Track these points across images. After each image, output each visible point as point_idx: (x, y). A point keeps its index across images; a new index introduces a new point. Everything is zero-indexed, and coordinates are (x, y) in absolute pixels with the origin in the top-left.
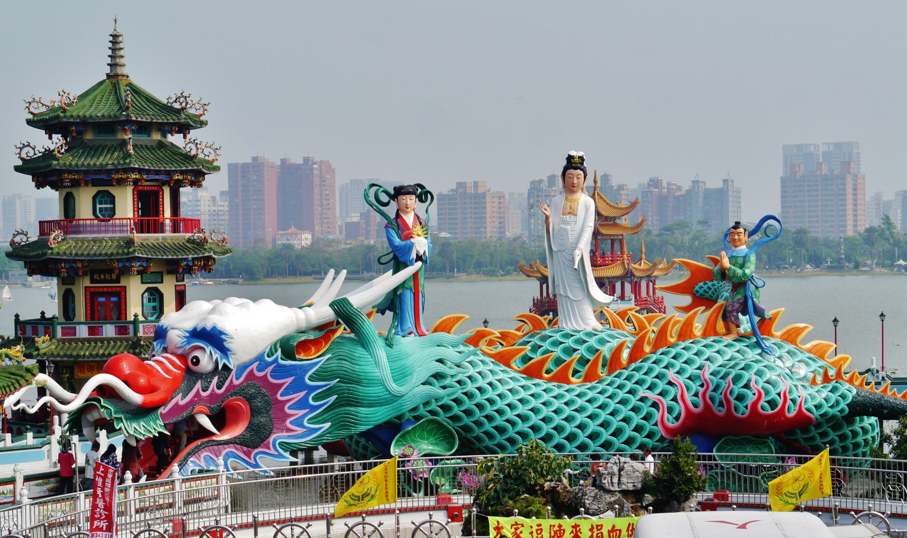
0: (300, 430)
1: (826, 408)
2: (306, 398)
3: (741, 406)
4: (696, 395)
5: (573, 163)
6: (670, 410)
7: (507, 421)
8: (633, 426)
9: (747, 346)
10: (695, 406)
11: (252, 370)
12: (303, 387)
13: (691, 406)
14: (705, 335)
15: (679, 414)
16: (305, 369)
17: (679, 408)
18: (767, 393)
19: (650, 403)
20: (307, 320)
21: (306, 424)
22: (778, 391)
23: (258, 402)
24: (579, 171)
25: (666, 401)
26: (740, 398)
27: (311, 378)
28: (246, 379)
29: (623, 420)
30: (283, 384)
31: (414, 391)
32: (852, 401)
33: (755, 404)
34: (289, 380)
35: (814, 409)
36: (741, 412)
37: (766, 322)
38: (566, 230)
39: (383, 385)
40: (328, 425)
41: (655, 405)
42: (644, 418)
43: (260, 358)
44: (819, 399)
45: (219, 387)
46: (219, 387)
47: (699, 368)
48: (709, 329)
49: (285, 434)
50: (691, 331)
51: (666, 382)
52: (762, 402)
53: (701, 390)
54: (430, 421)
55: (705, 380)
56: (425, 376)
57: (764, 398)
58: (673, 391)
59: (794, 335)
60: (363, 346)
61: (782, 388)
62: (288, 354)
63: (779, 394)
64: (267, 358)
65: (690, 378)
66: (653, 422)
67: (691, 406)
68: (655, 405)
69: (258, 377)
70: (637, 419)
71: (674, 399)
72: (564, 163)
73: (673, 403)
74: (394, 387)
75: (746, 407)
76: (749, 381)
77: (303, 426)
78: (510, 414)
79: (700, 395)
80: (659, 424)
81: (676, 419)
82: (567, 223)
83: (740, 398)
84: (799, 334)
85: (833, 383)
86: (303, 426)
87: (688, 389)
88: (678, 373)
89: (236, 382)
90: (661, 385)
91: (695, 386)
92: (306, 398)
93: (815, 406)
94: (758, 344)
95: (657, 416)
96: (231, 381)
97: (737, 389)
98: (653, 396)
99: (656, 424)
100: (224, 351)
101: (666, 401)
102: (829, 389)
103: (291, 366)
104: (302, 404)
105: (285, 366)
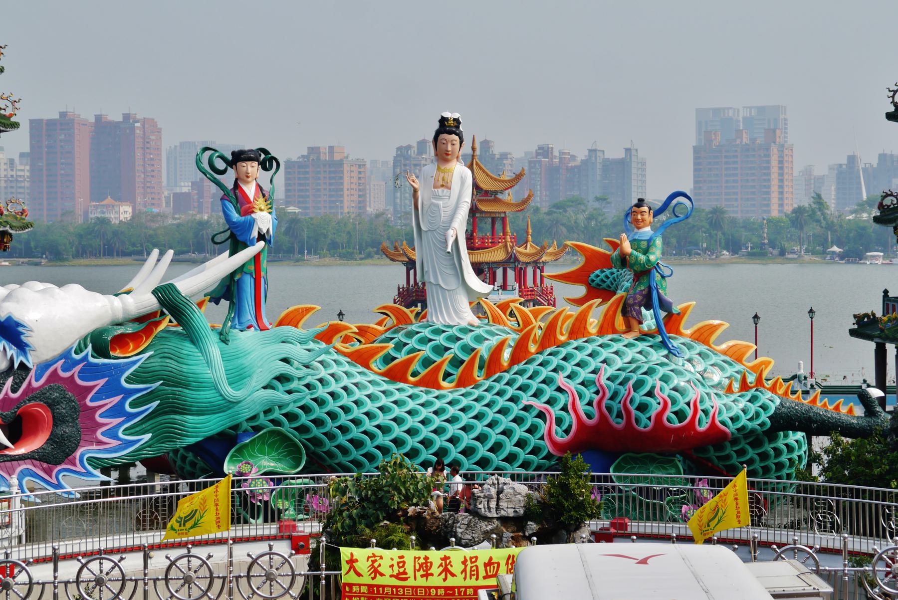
0: (114, 443)
1: (743, 421)
2: (121, 403)
3: (643, 417)
4: (590, 404)
6: (559, 421)
7: (365, 432)
8: (515, 439)
9: (651, 346)
10: (589, 416)
11: (56, 370)
13: (584, 417)
14: (601, 332)
15: (570, 426)
17: (569, 419)
18: (674, 402)
19: (535, 413)
20: (125, 310)
21: (121, 435)
22: (687, 400)
23: (63, 409)
24: (454, 137)
26: (643, 408)
28: (48, 381)
29: (503, 433)
31: (252, 397)
32: (775, 413)
33: (660, 415)
34: (102, 382)
35: (730, 422)
36: (643, 425)
38: (438, 206)
40: (148, 437)
41: (541, 415)
42: (529, 431)
44: (736, 410)
46: (14, 390)
47: (594, 372)
48: (605, 326)
49: (94, 447)
50: (585, 328)
51: (554, 387)
52: (668, 413)
53: (596, 398)
54: (272, 432)
55: (601, 386)
56: (267, 378)
57: (671, 409)
58: (562, 399)
59: (706, 334)
60: (193, 342)
61: (691, 396)
62: (101, 350)
63: (688, 404)
64: (74, 356)
65: (582, 384)
66: (539, 436)
67: (584, 417)
68: (541, 415)
70: (519, 432)
71: (564, 409)
72: (436, 126)
73: (563, 413)
74: (230, 392)
75: (649, 419)
78: (368, 425)
79: (595, 404)
80: (546, 438)
81: (567, 432)
82: (439, 197)
83: (643, 408)
87: (580, 396)
88: (569, 377)
89: (35, 384)
90: (549, 392)
92: (121, 403)
93: (731, 419)
95: (543, 428)
96: (30, 383)
98: (538, 404)
99: (542, 438)
101: (555, 411)
103: (104, 365)
105: (96, 365)
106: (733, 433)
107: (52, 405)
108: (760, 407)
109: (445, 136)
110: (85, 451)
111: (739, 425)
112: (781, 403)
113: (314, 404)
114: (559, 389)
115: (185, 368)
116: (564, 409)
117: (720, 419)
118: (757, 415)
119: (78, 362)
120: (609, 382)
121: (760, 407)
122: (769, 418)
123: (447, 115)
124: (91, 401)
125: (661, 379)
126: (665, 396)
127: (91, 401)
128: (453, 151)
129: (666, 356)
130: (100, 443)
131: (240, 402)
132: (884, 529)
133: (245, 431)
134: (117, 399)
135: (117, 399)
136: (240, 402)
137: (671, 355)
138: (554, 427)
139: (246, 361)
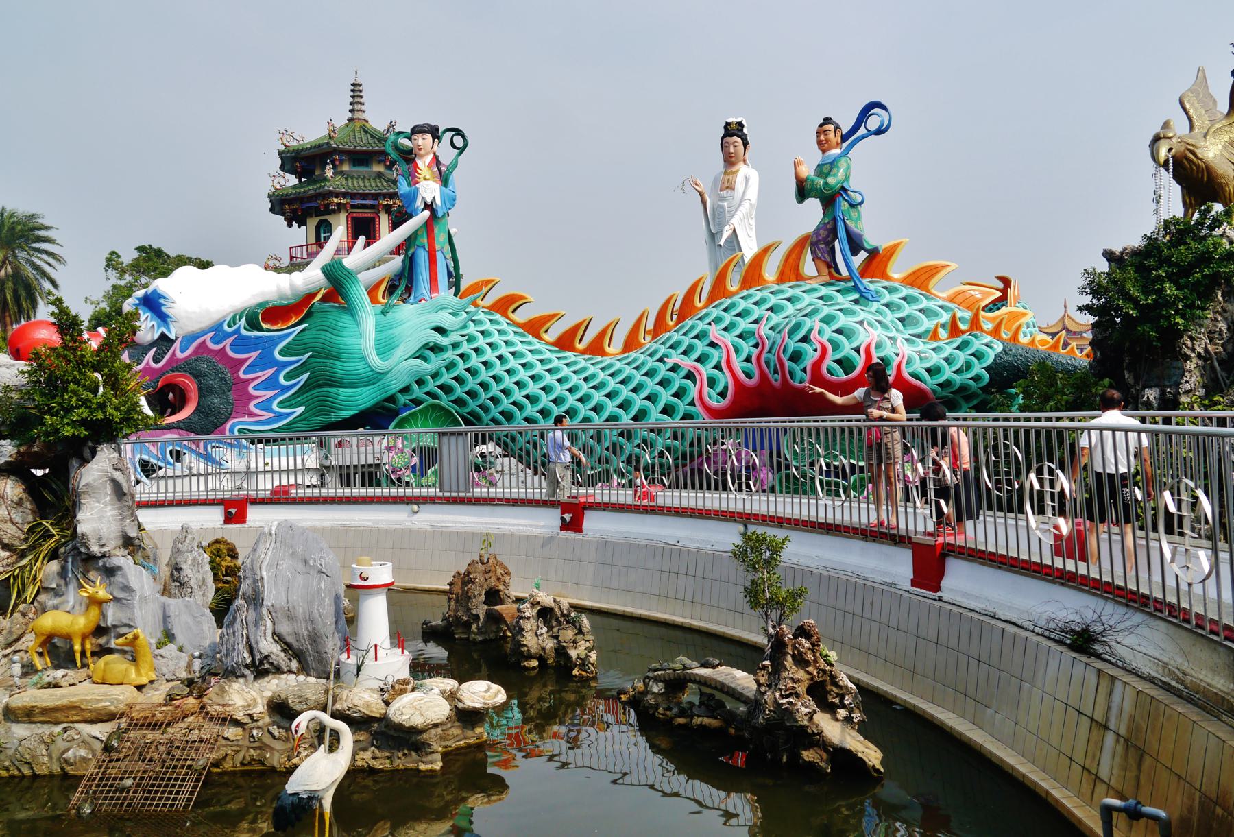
0: (267, 415)
1: (947, 374)
2: (274, 377)
3: (797, 369)
4: (748, 360)
5: (733, 130)
6: (712, 382)
7: (514, 403)
8: (661, 406)
9: (838, 291)
10: (748, 376)
11: (204, 342)
12: (273, 363)
13: (742, 377)
14: (781, 279)
15: (726, 388)
16: (274, 342)
17: (724, 379)
18: (836, 346)
19: (683, 373)
20: (292, 286)
21: (275, 407)
22: (855, 345)
23: (213, 381)
24: (735, 138)
25: (705, 370)
26: (796, 357)
27: (282, 353)
28: (195, 352)
29: (648, 398)
30: (246, 359)
31: (400, 367)
32: (995, 362)
33: (817, 364)
34: (255, 354)
35: (926, 375)
36: (798, 379)
37: (878, 259)
38: (722, 207)
39: (363, 358)
40: (303, 408)
41: (690, 376)
42: (676, 395)
43: (217, 328)
44: (935, 359)
45: (156, 360)
46: (156, 360)
47: (756, 322)
48: (787, 272)
49: (246, 419)
50: (760, 275)
51: (707, 342)
52: (828, 362)
53: (755, 352)
54: (433, 406)
55: (760, 337)
56: (414, 347)
57: (831, 356)
58: (715, 356)
59: (923, 277)
60: (352, 316)
61: (862, 339)
62: (253, 324)
63: (857, 350)
64: (226, 328)
65: (740, 336)
66: (689, 400)
67: (742, 377)
68: (690, 376)
69: (212, 351)
70: (665, 397)
71: (717, 367)
72: (722, 132)
73: (716, 372)
74: (376, 361)
75: (804, 370)
76: (810, 330)
77: (270, 410)
78: (518, 395)
79: (754, 359)
80: (696, 402)
81: (722, 394)
82: (723, 199)
83: (796, 357)
84: (932, 276)
85: (965, 336)
86: (270, 410)
87: (737, 350)
88: (725, 329)
89: (180, 355)
90: (701, 347)
91: (747, 347)
92: (274, 377)
93: (928, 370)
94: (856, 288)
95: (693, 391)
96: (174, 354)
97: (792, 345)
98: (687, 363)
99: (692, 403)
100: (163, 317)
101: (705, 370)
102: (956, 345)
103: (257, 338)
104: (271, 383)
105: (249, 338)
106: (934, 391)
107: (198, 375)
108: (973, 355)
109: (728, 139)
110: (235, 425)
111: (942, 380)
112: (1004, 350)
113: (468, 375)
114: (712, 345)
115: (338, 340)
116: (717, 367)
117: (910, 370)
118: (968, 366)
119: (228, 335)
120: (771, 332)
121: (973, 355)
122: (987, 369)
123: (729, 120)
124: (245, 373)
125: (821, 321)
126: (824, 340)
127: (245, 373)
128: (736, 153)
129: (856, 302)
130: (252, 415)
131: (386, 373)
132: (708, 477)
133: (405, 405)
134: (271, 371)
135: (271, 371)
136: (386, 373)
137: (862, 300)
138: (706, 388)
139: (396, 331)
